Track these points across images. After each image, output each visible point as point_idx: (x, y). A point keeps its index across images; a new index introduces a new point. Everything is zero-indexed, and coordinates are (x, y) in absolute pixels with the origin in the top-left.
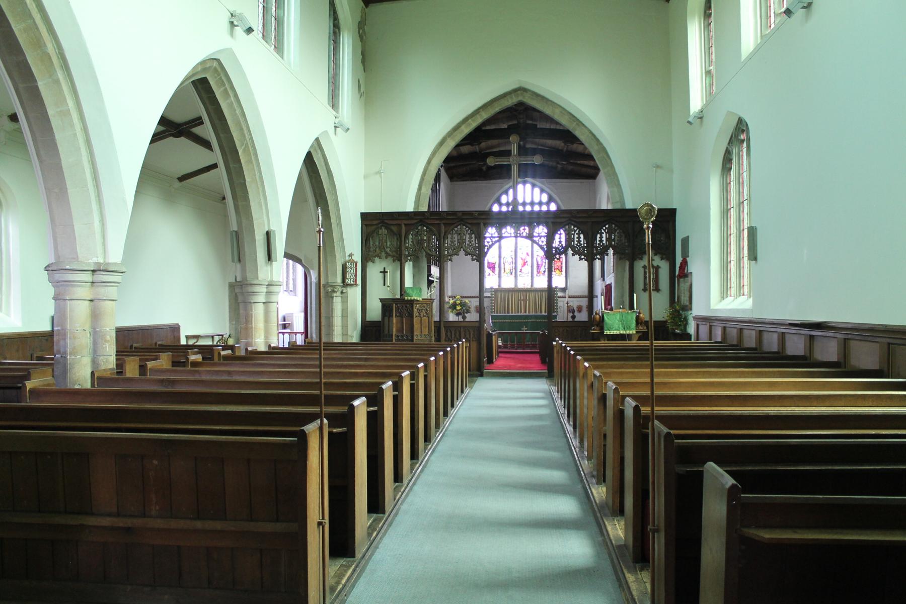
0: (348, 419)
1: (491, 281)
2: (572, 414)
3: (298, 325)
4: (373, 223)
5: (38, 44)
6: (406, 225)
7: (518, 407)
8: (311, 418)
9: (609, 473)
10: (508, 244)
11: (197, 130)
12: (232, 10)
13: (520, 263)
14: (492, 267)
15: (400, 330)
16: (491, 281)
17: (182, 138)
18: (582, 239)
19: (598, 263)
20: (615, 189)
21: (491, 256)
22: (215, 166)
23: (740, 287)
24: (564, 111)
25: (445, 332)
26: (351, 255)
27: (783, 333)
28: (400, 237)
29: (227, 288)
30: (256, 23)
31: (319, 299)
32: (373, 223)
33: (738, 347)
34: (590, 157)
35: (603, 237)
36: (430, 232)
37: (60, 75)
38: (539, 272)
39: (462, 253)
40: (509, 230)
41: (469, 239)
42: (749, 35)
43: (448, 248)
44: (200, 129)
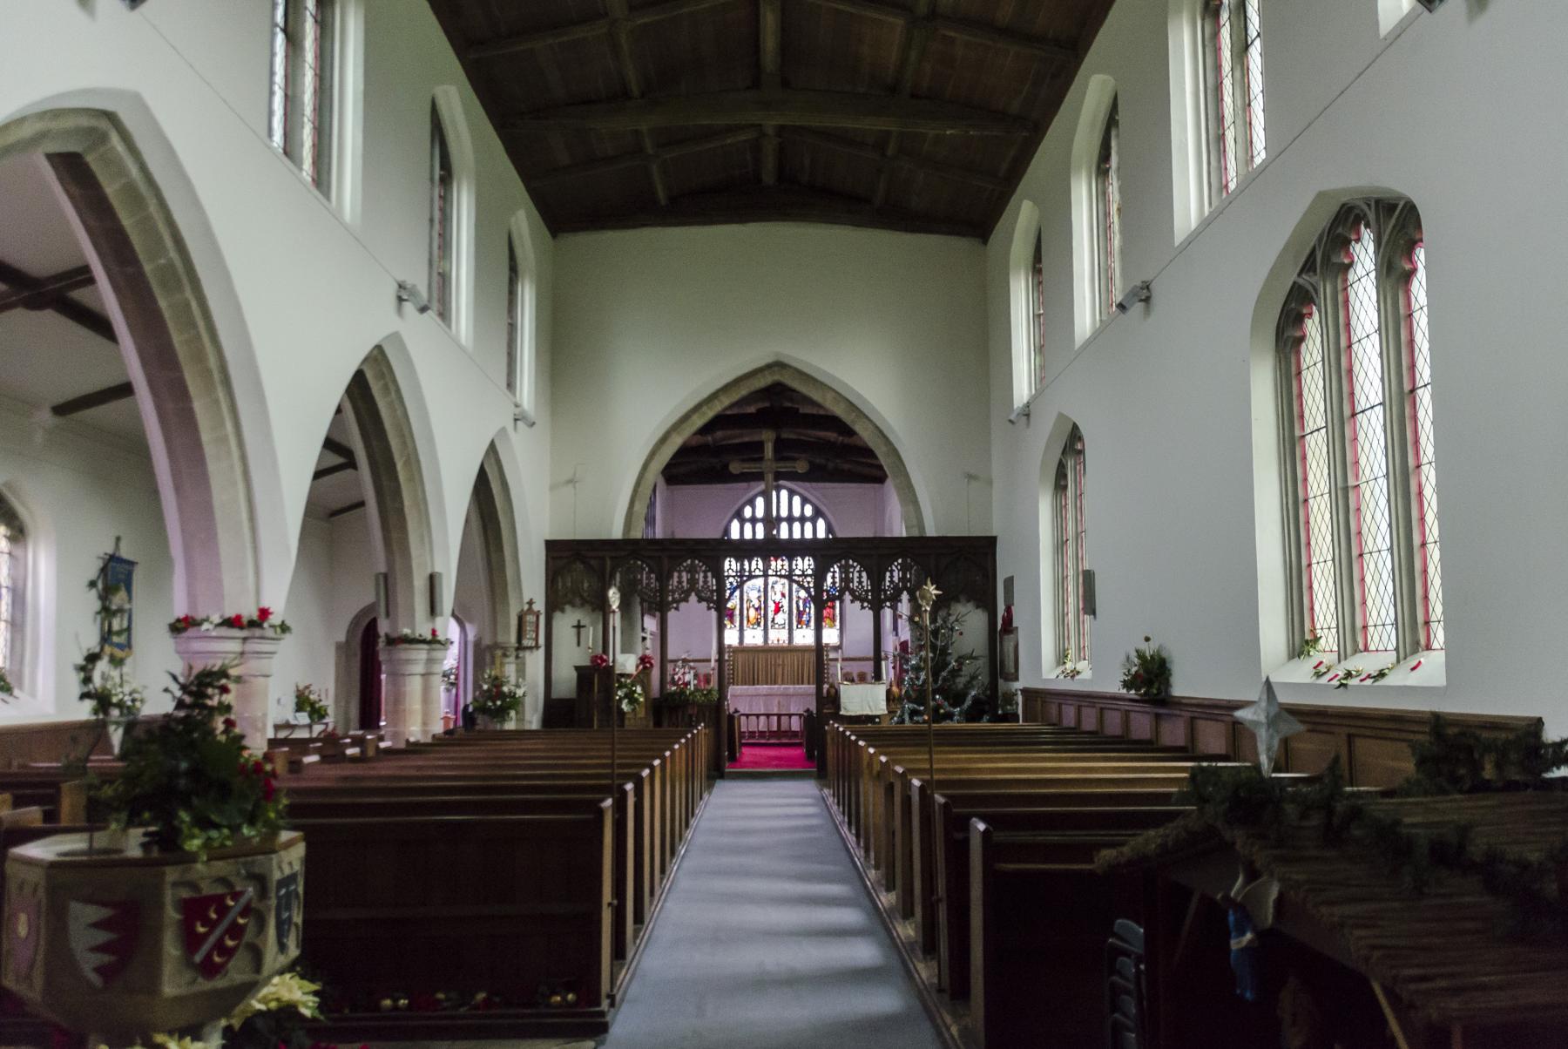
1: (731, 637)
2: (854, 817)
5: (200, 357)
6: (612, 558)
7: (778, 817)
9: (899, 883)
11: (80, 295)
12: (401, 278)
13: (772, 606)
18: (864, 579)
19: (887, 614)
20: (911, 508)
24: (839, 397)
26: (531, 603)
27: (1127, 712)
29: (333, 649)
35: (894, 575)
37: (221, 394)
38: (799, 622)
39: (693, 598)
41: (706, 580)
42: (1085, 316)
43: (673, 592)
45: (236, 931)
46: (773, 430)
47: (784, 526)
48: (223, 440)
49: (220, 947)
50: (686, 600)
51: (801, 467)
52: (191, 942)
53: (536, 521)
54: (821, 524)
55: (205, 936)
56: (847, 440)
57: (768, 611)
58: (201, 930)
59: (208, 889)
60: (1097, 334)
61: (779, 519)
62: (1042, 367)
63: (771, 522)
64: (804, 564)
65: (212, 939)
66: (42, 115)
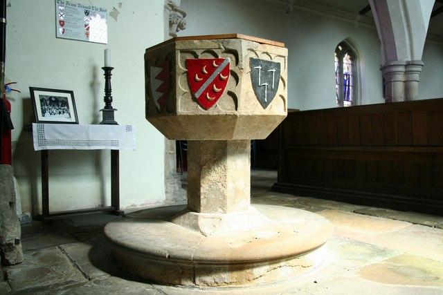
22: (183, 51)
45: (226, 71)
49: (210, 89)
52: (193, 86)
55: (201, 83)
58: (197, 78)
62: (171, 70)
65: (205, 85)
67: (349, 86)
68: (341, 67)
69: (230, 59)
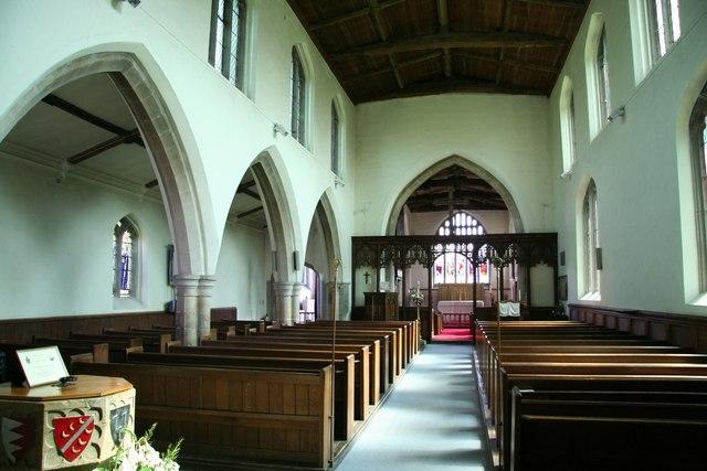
0: (344, 366)
3: (311, 307)
4: (359, 243)
8: (327, 364)
10: (450, 257)
14: (439, 269)
15: (377, 313)
16: (438, 279)
17: (161, 308)
21: (439, 262)
22: (49, 412)
23: (595, 285)
25: (407, 314)
28: (378, 253)
30: (289, 129)
31: (325, 293)
32: (359, 243)
33: (593, 325)
34: (498, 195)
36: (397, 249)
40: (451, 247)
44: (257, 202)
45: (91, 426)
46: (453, 187)
47: (458, 230)
48: (188, 193)
49: (77, 445)
50: (414, 263)
51: (465, 203)
52: (59, 442)
53: (346, 228)
54: (480, 228)
56: (487, 190)
57: (452, 268)
58: (64, 435)
59: (69, 415)
60: (601, 134)
61: (456, 227)
63: (452, 228)
64: (471, 247)
65: (72, 440)
66: (99, 54)
67: (127, 270)
68: (118, 248)
69: (94, 415)
